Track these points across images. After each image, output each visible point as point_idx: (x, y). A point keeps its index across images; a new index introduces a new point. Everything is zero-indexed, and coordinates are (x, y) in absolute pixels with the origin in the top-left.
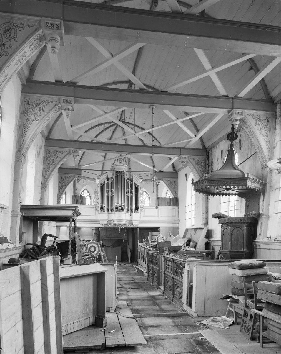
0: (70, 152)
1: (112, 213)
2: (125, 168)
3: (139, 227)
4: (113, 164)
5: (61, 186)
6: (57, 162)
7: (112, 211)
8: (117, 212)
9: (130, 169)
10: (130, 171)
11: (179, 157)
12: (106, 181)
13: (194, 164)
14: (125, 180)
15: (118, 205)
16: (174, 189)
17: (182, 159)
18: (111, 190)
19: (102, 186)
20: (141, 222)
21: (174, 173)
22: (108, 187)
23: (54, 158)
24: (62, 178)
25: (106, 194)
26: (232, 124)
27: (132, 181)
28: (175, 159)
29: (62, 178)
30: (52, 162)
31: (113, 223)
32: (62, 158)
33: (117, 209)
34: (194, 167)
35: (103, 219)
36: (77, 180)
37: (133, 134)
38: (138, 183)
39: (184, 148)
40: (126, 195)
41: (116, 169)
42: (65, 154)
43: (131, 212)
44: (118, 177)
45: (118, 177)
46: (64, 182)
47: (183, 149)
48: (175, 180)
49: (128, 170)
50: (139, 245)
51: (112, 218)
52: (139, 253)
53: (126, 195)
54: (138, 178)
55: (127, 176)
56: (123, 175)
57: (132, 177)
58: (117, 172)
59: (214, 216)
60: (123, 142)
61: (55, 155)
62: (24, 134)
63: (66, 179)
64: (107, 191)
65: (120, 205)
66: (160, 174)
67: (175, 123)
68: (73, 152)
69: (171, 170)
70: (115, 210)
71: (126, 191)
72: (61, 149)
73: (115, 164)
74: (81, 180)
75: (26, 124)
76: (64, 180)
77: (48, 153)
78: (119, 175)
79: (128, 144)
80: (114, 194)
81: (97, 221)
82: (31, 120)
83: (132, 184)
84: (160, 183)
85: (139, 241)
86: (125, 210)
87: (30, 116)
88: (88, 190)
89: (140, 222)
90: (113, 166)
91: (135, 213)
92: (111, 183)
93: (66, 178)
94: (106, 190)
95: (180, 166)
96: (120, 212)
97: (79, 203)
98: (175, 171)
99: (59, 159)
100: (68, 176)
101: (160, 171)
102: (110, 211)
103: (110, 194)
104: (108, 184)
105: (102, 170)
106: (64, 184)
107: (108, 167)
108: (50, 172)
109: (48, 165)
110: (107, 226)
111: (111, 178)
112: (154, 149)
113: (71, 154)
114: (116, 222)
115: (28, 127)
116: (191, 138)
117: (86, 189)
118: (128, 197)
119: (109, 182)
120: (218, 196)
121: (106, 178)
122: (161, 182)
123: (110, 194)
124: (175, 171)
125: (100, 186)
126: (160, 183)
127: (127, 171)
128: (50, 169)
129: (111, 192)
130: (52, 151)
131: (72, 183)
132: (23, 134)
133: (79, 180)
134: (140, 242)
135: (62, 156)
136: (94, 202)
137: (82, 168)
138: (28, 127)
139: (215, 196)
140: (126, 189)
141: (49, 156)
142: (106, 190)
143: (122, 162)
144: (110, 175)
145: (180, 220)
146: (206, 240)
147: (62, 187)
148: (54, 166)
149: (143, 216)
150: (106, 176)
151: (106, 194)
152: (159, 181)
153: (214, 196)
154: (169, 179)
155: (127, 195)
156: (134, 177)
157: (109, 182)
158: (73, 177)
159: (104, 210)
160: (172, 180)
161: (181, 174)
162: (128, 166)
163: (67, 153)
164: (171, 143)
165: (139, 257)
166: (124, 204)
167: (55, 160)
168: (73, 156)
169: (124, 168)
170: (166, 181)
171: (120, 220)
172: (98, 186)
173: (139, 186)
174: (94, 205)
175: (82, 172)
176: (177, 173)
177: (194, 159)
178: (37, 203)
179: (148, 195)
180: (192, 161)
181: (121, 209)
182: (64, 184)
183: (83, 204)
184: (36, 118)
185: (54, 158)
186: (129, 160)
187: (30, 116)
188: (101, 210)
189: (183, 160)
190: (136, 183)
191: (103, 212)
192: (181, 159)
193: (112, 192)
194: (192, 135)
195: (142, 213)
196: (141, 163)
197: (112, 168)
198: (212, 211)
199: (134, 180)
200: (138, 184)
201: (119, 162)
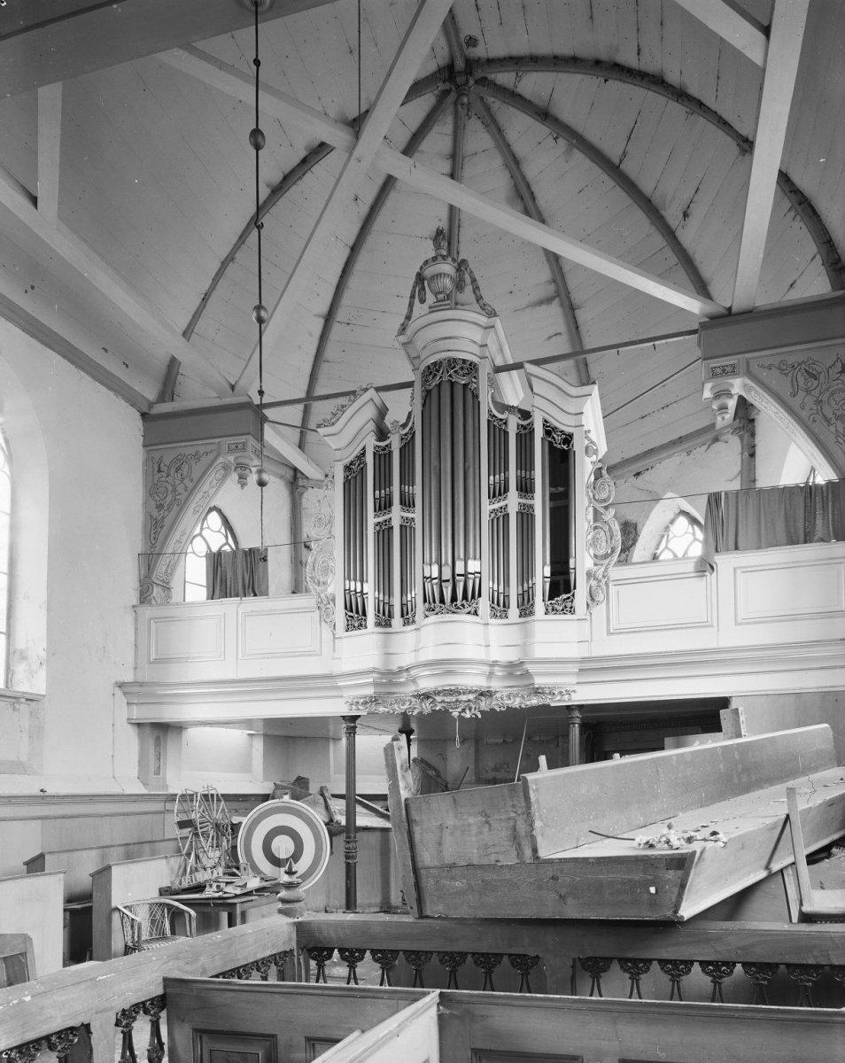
3: (581, 707)
5: (155, 513)
12: (371, 442)
20: (591, 667)
24: (159, 471)
25: (487, 507)
29: (159, 471)
31: (411, 689)
38: (563, 423)
43: (526, 609)
46: (170, 488)
72: (187, 449)
78: (439, 386)
86: (484, 604)
92: (401, 450)
93: (178, 464)
97: (241, 591)
100: (188, 451)
102: (397, 620)
103: (396, 514)
104: (383, 457)
118: (506, 516)
129: (402, 503)
147: (163, 518)
149: (609, 633)
150: (370, 412)
154: (796, 354)
158: (211, 456)
159: (364, 614)
183: (255, 595)
195: (599, 611)
200: (568, 430)
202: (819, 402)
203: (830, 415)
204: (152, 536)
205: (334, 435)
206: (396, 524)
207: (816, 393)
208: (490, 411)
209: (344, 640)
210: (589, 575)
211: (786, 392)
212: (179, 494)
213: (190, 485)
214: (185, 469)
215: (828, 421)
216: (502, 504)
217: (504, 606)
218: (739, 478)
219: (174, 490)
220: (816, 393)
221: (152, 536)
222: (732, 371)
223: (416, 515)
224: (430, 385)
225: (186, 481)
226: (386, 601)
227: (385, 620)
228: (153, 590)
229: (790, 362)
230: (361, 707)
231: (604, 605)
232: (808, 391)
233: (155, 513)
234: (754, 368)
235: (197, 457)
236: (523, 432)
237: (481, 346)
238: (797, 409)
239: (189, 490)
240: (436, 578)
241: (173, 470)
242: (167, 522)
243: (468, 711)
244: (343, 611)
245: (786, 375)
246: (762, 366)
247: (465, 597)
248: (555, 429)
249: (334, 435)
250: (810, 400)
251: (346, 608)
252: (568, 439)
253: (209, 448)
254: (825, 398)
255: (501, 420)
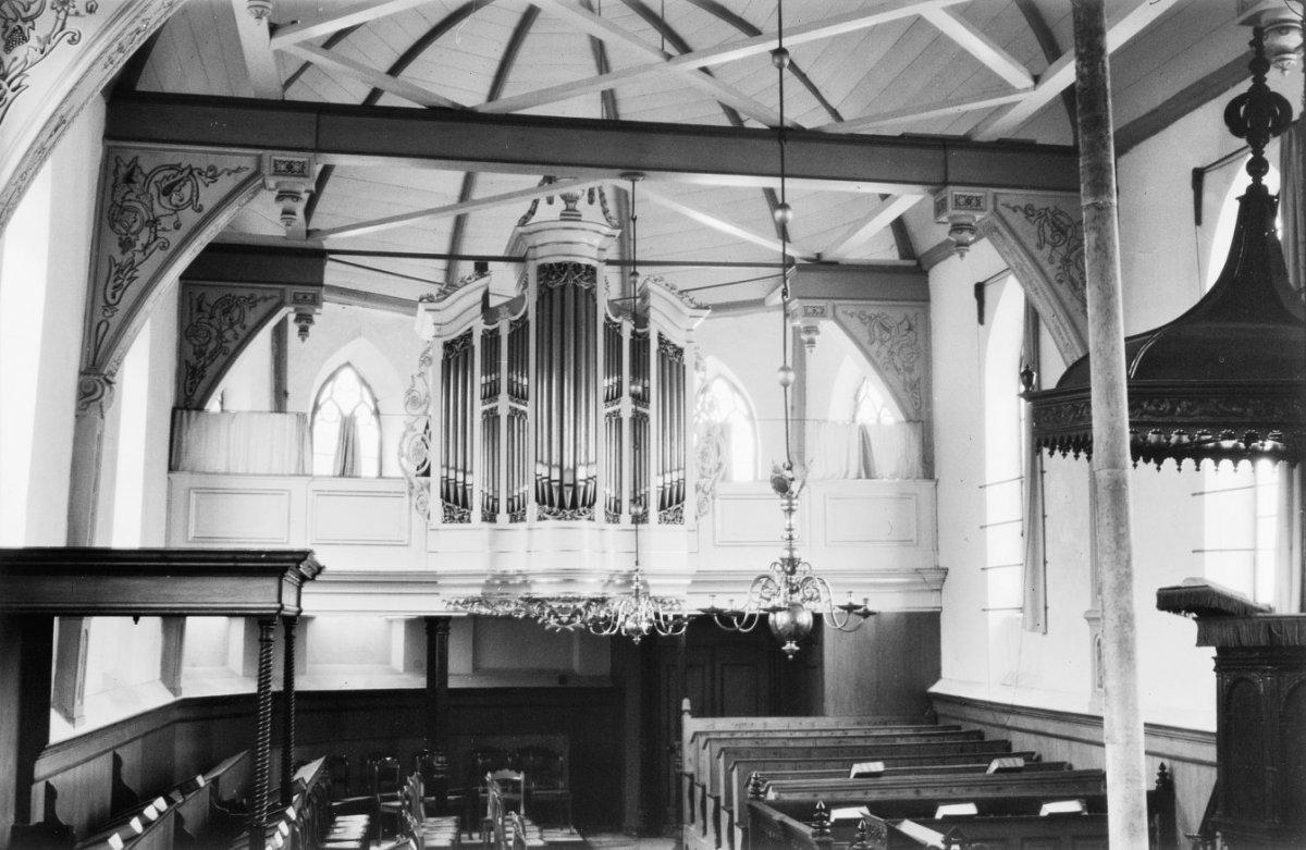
0: (257, 174)
1: (514, 525)
2: (597, 241)
4: (524, 221)
6: (175, 238)
7: (516, 514)
8: (551, 523)
9: (626, 240)
10: (627, 264)
11: (934, 193)
12: (479, 327)
13: (1032, 243)
14: (601, 320)
15: (556, 475)
16: (910, 370)
17: (957, 205)
18: (510, 381)
19: (456, 354)
21: (904, 278)
22: (491, 365)
23: (158, 211)
24: (200, 310)
26: (1253, 21)
27: (641, 319)
28: (908, 199)
29: (200, 310)
30: (144, 237)
31: (523, 593)
32: (206, 210)
33: (551, 504)
34: (1033, 259)
35: (465, 562)
36: (298, 319)
37: (648, 67)
38: (677, 338)
39: (964, 143)
40: (604, 410)
41: (541, 252)
42: (226, 184)
44: (557, 295)
45: (557, 295)
46: (214, 333)
47: (961, 147)
48: (911, 313)
49: (613, 254)
50: (688, 733)
51: (511, 564)
52: (687, 781)
53: (604, 410)
54: (673, 299)
55: (609, 287)
56: (584, 285)
57: (645, 296)
58: (547, 271)
59: (1171, 601)
60: (591, 109)
61: (167, 191)
62: (111, 301)
63: (225, 312)
64: (484, 385)
65: (568, 479)
66: (821, 277)
67: (915, 12)
68: (277, 173)
69: (888, 253)
70: (532, 508)
71: (605, 383)
72: (194, 156)
73: (534, 219)
74: (329, 313)
75: (6, 64)
76: (215, 322)
77: (120, 180)
78: (563, 288)
79: (623, 118)
80: (529, 409)
81: (426, 582)
82: (33, 42)
83: (640, 344)
84: (817, 332)
85: (686, 704)
86: (599, 509)
87: (31, 19)
88: (364, 372)
89: (694, 582)
90: (521, 229)
91: (664, 526)
92: (511, 337)
93: (227, 305)
94: (479, 379)
95: (941, 233)
96: (573, 523)
98: (912, 263)
99: (189, 217)
101: (818, 264)
102: (503, 517)
103: (504, 404)
104: (491, 339)
105: (453, 257)
106: (212, 346)
107: (490, 232)
108: (133, 290)
109: (123, 253)
110: (484, 611)
111: (514, 305)
112: (784, 148)
113: (263, 186)
114: (541, 590)
115: (14, 85)
116: (1004, 88)
117: (348, 364)
118: (620, 421)
119: (497, 330)
120: (1188, 463)
121: (478, 308)
122: (828, 329)
123: (504, 404)
124: (912, 263)
125: (438, 354)
126: (817, 332)
127: (609, 262)
128: (132, 279)
129: (510, 391)
130: (147, 165)
131: (263, 339)
132: (107, 302)
133: (309, 319)
134: (698, 712)
135: (209, 195)
136: (401, 454)
137: (327, 245)
138: (14, 85)
139: (1170, 462)
140: (608, 374)
141: (132, 196)
142: (479, 379)
143: (582, 205)
144: (505, 282)
145: (946, 571)
146: (1122, 531)
147: (204, 367)
148: (158, 256)
150: (478, 295)
151: (479, 408)
152: (812, 321)
153: (1159, 462)
154: (873, 309)
155: (611, 409)
156: (653, 301)
157: (497, 330)
159: (465, 505)
160: (895, 314)
161: (951, 281)
162: (618, 232)
163: (243, 175)
164: (893, 115)
165: (687, 811)
166: (592, 471)
167: (167, 222)
168: (281, 197)
169: (589, 242)
170: (854, 323)
171: (568, 576)
172: (426, 359)
173: (685, 355)
174: (401, 475)
175: (329, 265)
176: (925, 274)
177: (1028, 211)
178: (56, 538)
179: (743, 397)
180: (1016, 220)
181: (574, 505)
182: (212, 346)
184: (62, 29)
185: (158, 211)
186: (623, 198)
187: (31, 19)
188: (447, 510)
189: (964, 215)
190: (667, 337)
191: (461, 520)
192: (951, 211)
193: (518, 395)
194: (1016, 76)
196: (703, 214)
197: (518, 239)
198: (1155, 571)
199: (653, 314)
200: (680, 344)
201: (560, 205)
202: (891, 353)
203: (899, 366)
204: (188, 386)
205: (438, 310)
206: (503, 412)
207: (888, 344)
208: (606, 315)
209: (441, 533)
210: (697, 488)
211: (865, 340)
212: (227, 341)
213: (242, 334)
214: (236, 314)
215: (898, 370)
216: (616, 408)
217: (615, 510)
218: (660, 14)
219: (220, 334)
220: (888, 344)
221: (188, 386)
222: (822, 314)
223: (529, 409)
224: (553, 284)
225: (237, 328)
226: (491, 494)
227: (490, 515)
228: (103, 390)
229: (868, 313)
230: (459, 607)
231: (710, 515)
232: (883, 342)
233: (193, 360)
234: (839, 311)
235: (213, 175)
236: (637, 339)
237: (600, 249)
238: (874, 356)
239: (240, 338)
240: (555, 481)
241: (218, 312)
242: (210, 371)
243: (579, 617)
244: (440, 501)
245: (865, 324)
246: (846, 313)
247: (584, 504)
248: (668, 342)
249: (438, 310)
250: (884, 352)
251: (442, 497)
252: (679, 351)
253: (268, 294)
254: (895, 350)
255: (615, 324)
